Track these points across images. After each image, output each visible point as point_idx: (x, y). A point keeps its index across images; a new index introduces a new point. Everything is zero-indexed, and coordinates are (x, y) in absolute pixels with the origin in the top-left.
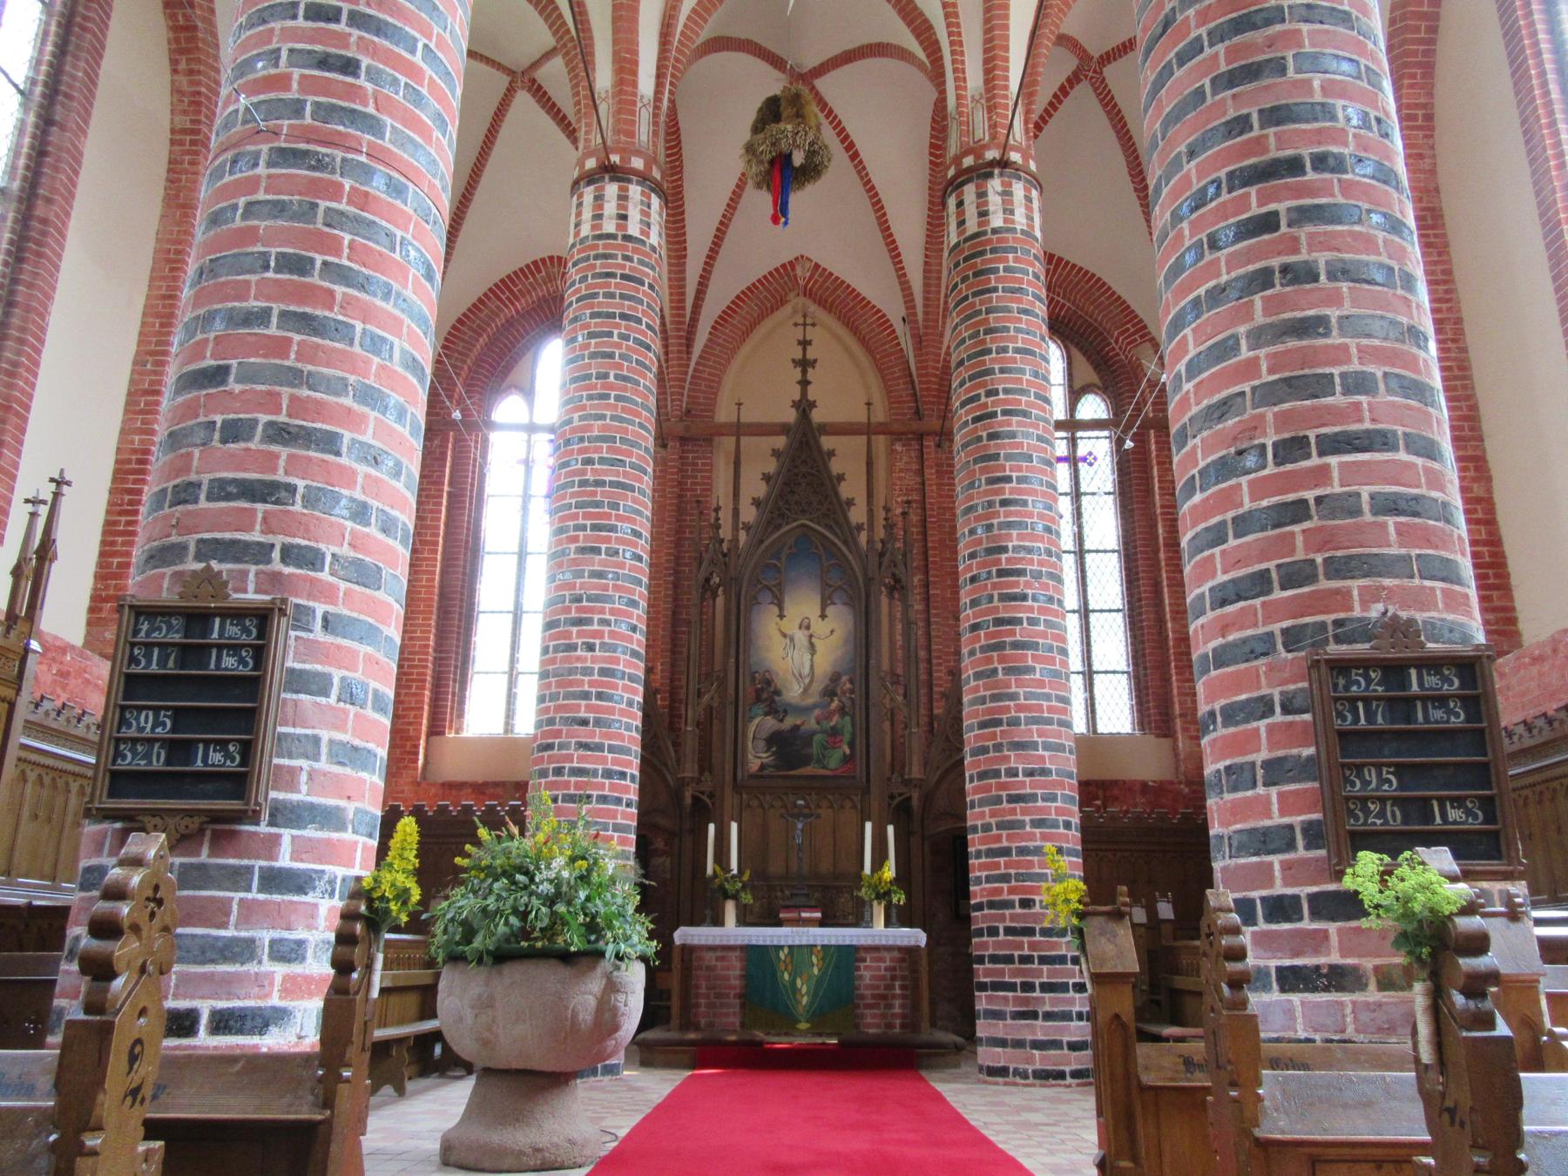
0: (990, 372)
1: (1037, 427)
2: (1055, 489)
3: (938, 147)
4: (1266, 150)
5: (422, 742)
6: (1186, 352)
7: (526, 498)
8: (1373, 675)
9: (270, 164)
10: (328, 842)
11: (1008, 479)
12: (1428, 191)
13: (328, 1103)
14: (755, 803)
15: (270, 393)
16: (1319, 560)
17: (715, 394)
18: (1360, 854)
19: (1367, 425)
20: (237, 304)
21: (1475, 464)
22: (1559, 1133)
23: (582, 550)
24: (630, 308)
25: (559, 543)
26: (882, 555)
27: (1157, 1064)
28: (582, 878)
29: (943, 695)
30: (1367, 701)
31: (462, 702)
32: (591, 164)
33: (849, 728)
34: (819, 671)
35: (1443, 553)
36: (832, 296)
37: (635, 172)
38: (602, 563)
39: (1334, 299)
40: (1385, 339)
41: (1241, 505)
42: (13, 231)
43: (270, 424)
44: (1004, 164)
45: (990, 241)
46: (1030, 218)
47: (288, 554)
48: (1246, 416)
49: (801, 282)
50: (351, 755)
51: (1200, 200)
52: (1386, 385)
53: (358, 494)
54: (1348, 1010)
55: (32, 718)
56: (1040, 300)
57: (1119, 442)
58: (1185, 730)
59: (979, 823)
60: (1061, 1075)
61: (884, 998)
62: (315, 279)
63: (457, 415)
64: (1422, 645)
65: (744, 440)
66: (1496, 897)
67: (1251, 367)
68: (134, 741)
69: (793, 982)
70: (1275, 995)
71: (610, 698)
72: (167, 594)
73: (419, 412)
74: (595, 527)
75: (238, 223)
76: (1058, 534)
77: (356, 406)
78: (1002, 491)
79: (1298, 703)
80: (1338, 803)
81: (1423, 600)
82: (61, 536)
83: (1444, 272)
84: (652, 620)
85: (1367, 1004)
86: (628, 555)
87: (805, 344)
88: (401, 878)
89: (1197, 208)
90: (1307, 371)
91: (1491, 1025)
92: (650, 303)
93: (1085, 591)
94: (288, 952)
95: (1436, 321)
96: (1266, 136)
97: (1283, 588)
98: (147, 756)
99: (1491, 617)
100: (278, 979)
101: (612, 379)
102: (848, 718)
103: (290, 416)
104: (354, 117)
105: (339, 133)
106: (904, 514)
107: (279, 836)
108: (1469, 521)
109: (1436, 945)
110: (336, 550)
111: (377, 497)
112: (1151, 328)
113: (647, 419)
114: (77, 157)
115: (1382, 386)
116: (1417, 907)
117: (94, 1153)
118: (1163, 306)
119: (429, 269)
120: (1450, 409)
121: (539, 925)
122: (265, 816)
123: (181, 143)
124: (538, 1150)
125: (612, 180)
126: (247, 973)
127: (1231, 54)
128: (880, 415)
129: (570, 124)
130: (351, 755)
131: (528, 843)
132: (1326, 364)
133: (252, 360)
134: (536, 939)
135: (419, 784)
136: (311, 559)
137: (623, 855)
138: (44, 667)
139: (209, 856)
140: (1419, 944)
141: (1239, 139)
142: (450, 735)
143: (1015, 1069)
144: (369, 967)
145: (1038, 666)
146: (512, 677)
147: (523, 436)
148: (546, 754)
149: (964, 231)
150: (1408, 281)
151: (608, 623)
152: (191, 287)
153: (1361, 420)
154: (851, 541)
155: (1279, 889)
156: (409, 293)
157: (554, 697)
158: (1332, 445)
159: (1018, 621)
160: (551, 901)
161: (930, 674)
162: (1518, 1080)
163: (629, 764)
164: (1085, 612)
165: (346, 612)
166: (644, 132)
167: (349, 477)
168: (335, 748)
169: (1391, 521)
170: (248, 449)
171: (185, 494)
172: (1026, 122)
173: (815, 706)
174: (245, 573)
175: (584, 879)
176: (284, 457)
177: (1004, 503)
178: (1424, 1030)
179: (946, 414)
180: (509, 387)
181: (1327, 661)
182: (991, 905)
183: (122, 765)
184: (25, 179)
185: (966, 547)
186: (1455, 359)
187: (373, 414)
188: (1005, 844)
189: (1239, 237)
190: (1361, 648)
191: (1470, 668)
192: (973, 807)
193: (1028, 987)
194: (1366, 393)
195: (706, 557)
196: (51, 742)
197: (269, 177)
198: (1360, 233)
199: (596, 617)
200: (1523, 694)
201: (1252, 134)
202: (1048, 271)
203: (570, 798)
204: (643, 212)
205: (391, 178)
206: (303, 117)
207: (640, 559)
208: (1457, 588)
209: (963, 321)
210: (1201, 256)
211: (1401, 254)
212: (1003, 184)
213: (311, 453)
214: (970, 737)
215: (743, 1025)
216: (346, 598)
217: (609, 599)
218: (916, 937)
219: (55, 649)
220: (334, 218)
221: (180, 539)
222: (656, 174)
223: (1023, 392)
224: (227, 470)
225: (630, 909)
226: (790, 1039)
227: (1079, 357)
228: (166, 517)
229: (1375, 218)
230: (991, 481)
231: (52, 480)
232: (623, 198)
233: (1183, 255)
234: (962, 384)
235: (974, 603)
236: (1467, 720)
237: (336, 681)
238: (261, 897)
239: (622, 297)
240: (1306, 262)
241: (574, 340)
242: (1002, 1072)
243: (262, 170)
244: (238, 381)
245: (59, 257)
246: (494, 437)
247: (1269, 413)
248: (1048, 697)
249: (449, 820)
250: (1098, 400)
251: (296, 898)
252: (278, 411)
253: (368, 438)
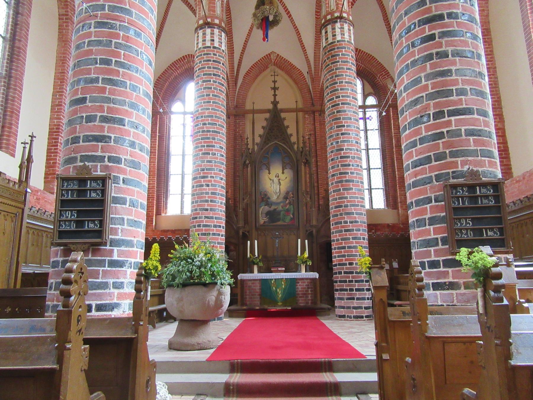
0: (337, 90)
1: (353, 108)
2: (359, 129)
3: (318, 12)
4: (431, 12)
5: (154, 217)
6: (404, 83)
7: (184, 137)
8: (465, 189)
9: (95, 28)
10: (129, 251)
11: (344, 126)
12: (485, 23)
13: (136, 332)
14: (262, 234)
15: (100, 106)
16: (447, 152)
17: (245, 100)
18: (461, 249)
19: (464, 106)
20: (88, 76)
21: (499, 117)
22: (523, 333)
23: (204, 154)
24: (216, 72)
25: (196, 151)
26: (302, 152)
27: (393, 314)
28: (209, 260)
29: (323, 197)
30: (462, 198)
31: (166, 204)
32: (201, 22)
33: (292, 209)
34: (282, 191)
35: (489, 149)
36: (283, 65)
37: (216, 25)
38: (210, 158)
39: (454, 63)
40: (471, 76)
41: (422, 134)
42: (9, 52)
43: (101, 116)
44: (341, 18)
45: (336, 45)
46: (350, 37)
47: (110, 159)
48: (424, 104)
49: (273, 61)
50: (134, 223)
51: (409, 30)
52: (471, 92)
53: (131, 139)
54: (455, 296)
55: (29, 213)
56: (354, 65)
57: (380, 114)
58: (401, 207)
59: (335, 239)
60: (362, 317)
61: (305, 295)
62: (113, 67)
63: (161, 110)
64: (481, 179)
65: (255, 115)
66: (503, 259)
67: (426, 87)
68: (65, 221)
69: (277, 290)
70: (431, 292)
71: (215, 202)
72: (72, 173)
73: (150, 110)
74: (207, 146)
75: (86, 48)
76: (360, 144)
77: (129, 109)
78: (342, 130)
79: (440, 199)
80: (452, 230)
81: (481, 164)
82: (34, 154)
83: (490, 51)
84: (227, 176)
85: (461, 294)
86: (219, 155)
87: (275, 82)
88: (155, 262)
89: (408, 33)
90: (444, 88)
91: (502, 301)
92: (223, 70)
93: (369, 162)
94: (118, 286)
95: (488, 68)
96: (431, 7)
97: (435, 161)
98: (70, 226)
99: (503, 168)
100: (116, 294)
101: (211, 96)
102: (292, 206)
103: (108, 113)
104: (122, 10)
105: (118, 15)
106: (309, 138)
107: (113, 250)
108: (497, 136)
109: (485, 277)
110: (126, 157)
111: (138, 139)
112: (391, 73)
113: (223, 109)
114: (28, 24)
115: (469, 93)
116: (479, 265)
117: (69, 349)
118: (396, 67)
119: (150, 62)
120: (492, 98)
121: (196, 275)
122: (108, 243)
123: (62, 19)
124: (199, 344)
125: (208, 28)
126: (106, 293)
128: (300, 105)
129: (193, 8)
130: (134, 223)
131: (191, 249)
132: (450, 86)
133: (94, 95)
134: (195, 279)
135: (154, 231)
136: (117, 160)
137: (222, 252)
138: (32, 197)
139: (92, 256)
140: (480, 277)
141: (422, 8)
142: (163, 215)
143: (348, 316)
144: (146, 290)
145: (354, 188)
146: (182, 195)
147: (182, 116)
148: (195, 220)
149: (328, 42)
150: (479, 56)
151: (213, 177)
152: (72, 70)
153: (462, 105)
155: (433, 258)
156: (144, 70)
157: (197, 202)
158: (452, 113)
159: (347, 173)
160: (199, 267)
161: (318, 191)
162: (510, 317)
163: (222, 223)
164: (369, 169)
165: (130, 177)
167: (128, 133)
168: (129, 221)
169: (471, 138)
170: (95, 125)
171: (75, 140)
172: (348, 3)
173: (281, 202)
174: (97, 166)
175: (210, 260)
176: (107, 127)
177: (342, 134)
178: (481, 303)
179: (322, 104)
180: (177, 99)
181: (450, 185)
182: (339, 265)
183: (62, 229)
184: (11, 33)
185: (330, 149)
186: (494, 81)
187: (135, 112)
188: (344, 245)
189: (422, 43)
190: (461, 180)
191: (496, 186)
192: (333, 234)
193: (351, 290)
194: (464, 96)
195: (244, 155)
196: (36, 221)
197: (95, 32)
198: (463, 40)
199: (209, 176)
200: (512, 193)
201: (427, 6)
202: (356, 55)
204: (219, 38)
205: (136, 31)
206: (105, 10)
207: (223, 156)
208: (493, 160)
209: (328, 73)
210: (408, 50)
211: (476, 47)
212: (341, 25)
213: (115, 126)
214: (332, 211)
215: (260, 303)
216: (129, 173)
217: (213, 169)
218: (316, 275)
219: (35, 191)
220: (118, 46)
221: (75, 155)
222: (223, 25)
223: (348, 97)
224: (89, 132)
225: (225, 269)
226: (276, 308)
227: (366, 83)
228: (69, 148)
229: (468, 35)
230: (337, 127)
231: (30, 136)
232: (212, 34)
233: (403, 49)
234: (328, 94)
235: (333, 167)
236: (495, 203)
237: (128, 200)
238: (109, 269)
239: (213, 68)
240: (444, 51)
241: (198, 83)
242: (343, 316)
243: (92, 29)
244: (89, 102)
245: (25, 60)
246: (173, 116)
247: (432, 103)
248: (357, 198)
249: (166, 241)
250: (373, 98)
251: (120, 269)
252: (104, 112)
253: (133, 120)
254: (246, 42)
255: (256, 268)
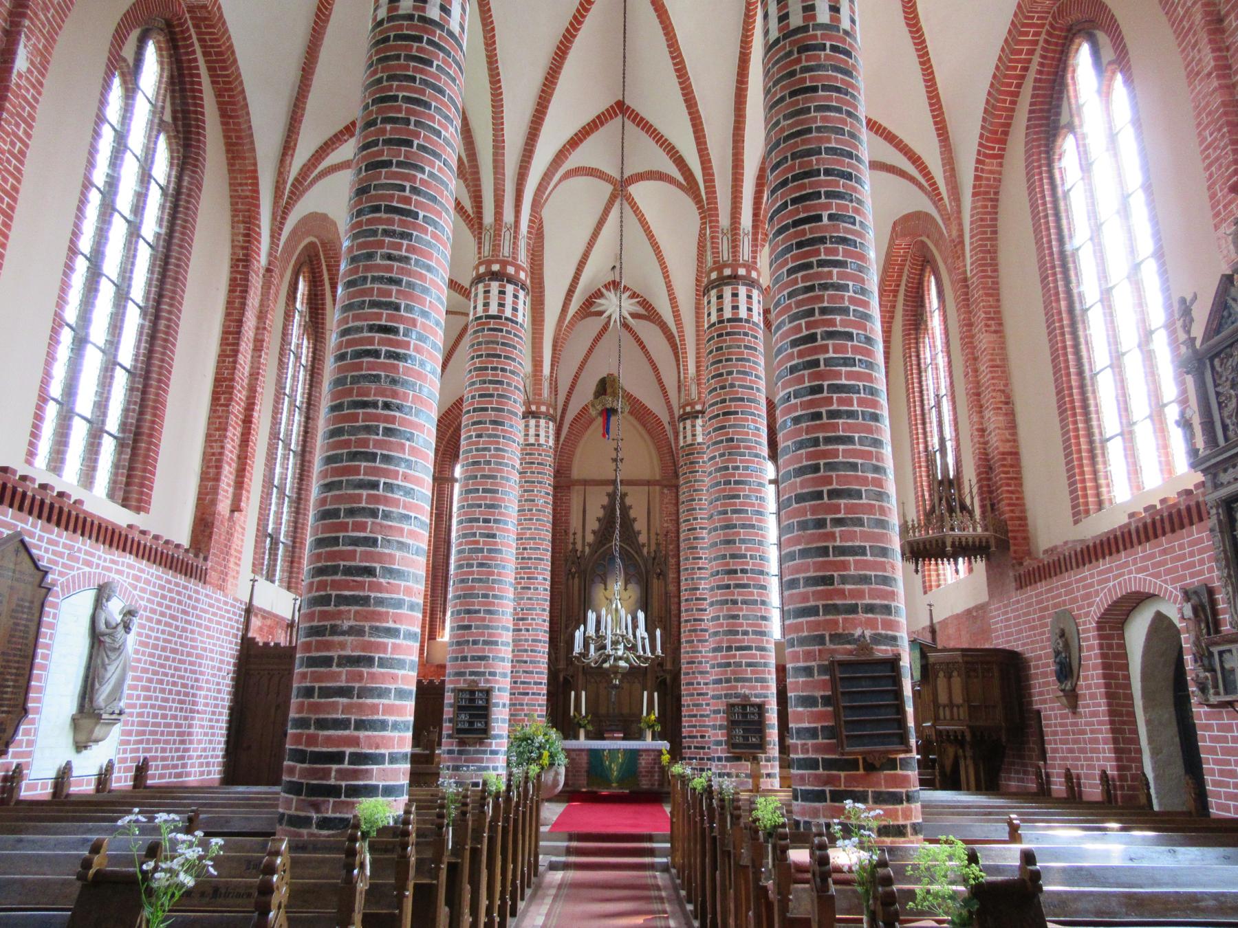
23: (523, 588)
37: (542, 413)
39: (741, 610)
44: (734, 278)
72: (462, 685)
80: (730, 736)
127: (725, 535)
142: (439, 639)
154: (639, 552)
158: (738, 649)
166: (546, 392)
177: (699, 569)
203: (520, 694)
232: (537, 426)
235: (686, 611)
254: (576, 377)
255: (582, 733)
